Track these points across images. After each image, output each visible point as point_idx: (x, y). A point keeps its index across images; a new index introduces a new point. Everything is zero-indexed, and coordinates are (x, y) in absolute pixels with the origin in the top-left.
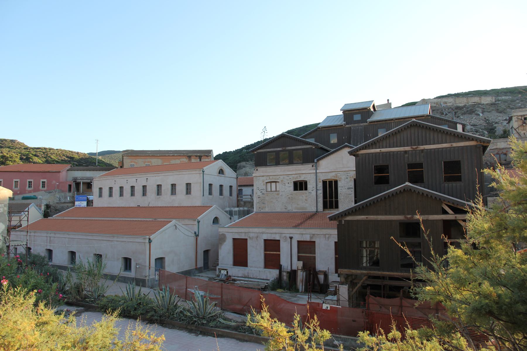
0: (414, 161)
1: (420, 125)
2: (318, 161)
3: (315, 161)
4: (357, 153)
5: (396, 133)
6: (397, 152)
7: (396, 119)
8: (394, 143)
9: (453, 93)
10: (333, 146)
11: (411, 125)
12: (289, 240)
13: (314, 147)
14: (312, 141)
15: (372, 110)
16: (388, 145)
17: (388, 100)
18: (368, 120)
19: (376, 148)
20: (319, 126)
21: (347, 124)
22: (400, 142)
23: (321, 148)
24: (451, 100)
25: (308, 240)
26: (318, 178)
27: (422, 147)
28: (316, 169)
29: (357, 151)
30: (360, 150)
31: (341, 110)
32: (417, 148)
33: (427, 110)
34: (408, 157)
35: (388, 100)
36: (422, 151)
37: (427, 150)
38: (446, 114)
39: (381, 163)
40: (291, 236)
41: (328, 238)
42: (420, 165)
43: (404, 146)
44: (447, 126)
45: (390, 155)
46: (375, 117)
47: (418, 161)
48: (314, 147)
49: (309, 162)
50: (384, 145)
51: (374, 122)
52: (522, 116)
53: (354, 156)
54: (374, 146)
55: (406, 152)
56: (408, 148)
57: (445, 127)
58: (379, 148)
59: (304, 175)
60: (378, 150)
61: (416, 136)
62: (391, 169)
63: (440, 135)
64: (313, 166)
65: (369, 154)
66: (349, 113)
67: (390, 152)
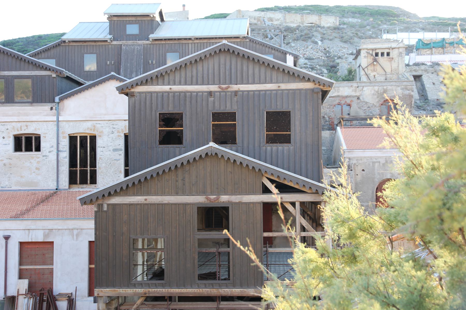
2: (61, 99)
3: (57, 99)
4: (132, 90)
5: (196, 60)
6: (180, 92)
7: (197, 39)
8: (192, 77)
9: (283, 6)
10: (89, 75)
11: (220, 50)
12: (4, 241)
13: (54, 75)
14: (51, 63)
16: (183, 80)
17: (184, 6)
18: (152, 36)
19: (163, 84)
21: (115, 39)
22: (203, 77)
23: (68, 78)
24: (278, 16)
25: (40, 239)
26: (61, 131)
27: (235, 87)
28: (58, 115)
30: (137, 85)
31: (105, 14)
32: (229, 87)
35: (184, 6)
36: (236, 93)
37: (243, 91)
38: (272, 38)
39: (170, 109)
40: (7, 233)
41: (77, 235)
42: (232, 116)
43: (208, 84)
45: (185, 96)
48: (54, 75)
49: (45, 102)
51: (161, 40)
52: (373, 50)
53: (127, 95)
54: (160, 81)
55: (210, 93)
56: (214, 88)
58: (169, 84)
59: (34, 125)
60: (166, 88)
61: (228, 67)
62: (186, 121)
64: (52, 109)
65: (151, 93)
67: (185, 92)
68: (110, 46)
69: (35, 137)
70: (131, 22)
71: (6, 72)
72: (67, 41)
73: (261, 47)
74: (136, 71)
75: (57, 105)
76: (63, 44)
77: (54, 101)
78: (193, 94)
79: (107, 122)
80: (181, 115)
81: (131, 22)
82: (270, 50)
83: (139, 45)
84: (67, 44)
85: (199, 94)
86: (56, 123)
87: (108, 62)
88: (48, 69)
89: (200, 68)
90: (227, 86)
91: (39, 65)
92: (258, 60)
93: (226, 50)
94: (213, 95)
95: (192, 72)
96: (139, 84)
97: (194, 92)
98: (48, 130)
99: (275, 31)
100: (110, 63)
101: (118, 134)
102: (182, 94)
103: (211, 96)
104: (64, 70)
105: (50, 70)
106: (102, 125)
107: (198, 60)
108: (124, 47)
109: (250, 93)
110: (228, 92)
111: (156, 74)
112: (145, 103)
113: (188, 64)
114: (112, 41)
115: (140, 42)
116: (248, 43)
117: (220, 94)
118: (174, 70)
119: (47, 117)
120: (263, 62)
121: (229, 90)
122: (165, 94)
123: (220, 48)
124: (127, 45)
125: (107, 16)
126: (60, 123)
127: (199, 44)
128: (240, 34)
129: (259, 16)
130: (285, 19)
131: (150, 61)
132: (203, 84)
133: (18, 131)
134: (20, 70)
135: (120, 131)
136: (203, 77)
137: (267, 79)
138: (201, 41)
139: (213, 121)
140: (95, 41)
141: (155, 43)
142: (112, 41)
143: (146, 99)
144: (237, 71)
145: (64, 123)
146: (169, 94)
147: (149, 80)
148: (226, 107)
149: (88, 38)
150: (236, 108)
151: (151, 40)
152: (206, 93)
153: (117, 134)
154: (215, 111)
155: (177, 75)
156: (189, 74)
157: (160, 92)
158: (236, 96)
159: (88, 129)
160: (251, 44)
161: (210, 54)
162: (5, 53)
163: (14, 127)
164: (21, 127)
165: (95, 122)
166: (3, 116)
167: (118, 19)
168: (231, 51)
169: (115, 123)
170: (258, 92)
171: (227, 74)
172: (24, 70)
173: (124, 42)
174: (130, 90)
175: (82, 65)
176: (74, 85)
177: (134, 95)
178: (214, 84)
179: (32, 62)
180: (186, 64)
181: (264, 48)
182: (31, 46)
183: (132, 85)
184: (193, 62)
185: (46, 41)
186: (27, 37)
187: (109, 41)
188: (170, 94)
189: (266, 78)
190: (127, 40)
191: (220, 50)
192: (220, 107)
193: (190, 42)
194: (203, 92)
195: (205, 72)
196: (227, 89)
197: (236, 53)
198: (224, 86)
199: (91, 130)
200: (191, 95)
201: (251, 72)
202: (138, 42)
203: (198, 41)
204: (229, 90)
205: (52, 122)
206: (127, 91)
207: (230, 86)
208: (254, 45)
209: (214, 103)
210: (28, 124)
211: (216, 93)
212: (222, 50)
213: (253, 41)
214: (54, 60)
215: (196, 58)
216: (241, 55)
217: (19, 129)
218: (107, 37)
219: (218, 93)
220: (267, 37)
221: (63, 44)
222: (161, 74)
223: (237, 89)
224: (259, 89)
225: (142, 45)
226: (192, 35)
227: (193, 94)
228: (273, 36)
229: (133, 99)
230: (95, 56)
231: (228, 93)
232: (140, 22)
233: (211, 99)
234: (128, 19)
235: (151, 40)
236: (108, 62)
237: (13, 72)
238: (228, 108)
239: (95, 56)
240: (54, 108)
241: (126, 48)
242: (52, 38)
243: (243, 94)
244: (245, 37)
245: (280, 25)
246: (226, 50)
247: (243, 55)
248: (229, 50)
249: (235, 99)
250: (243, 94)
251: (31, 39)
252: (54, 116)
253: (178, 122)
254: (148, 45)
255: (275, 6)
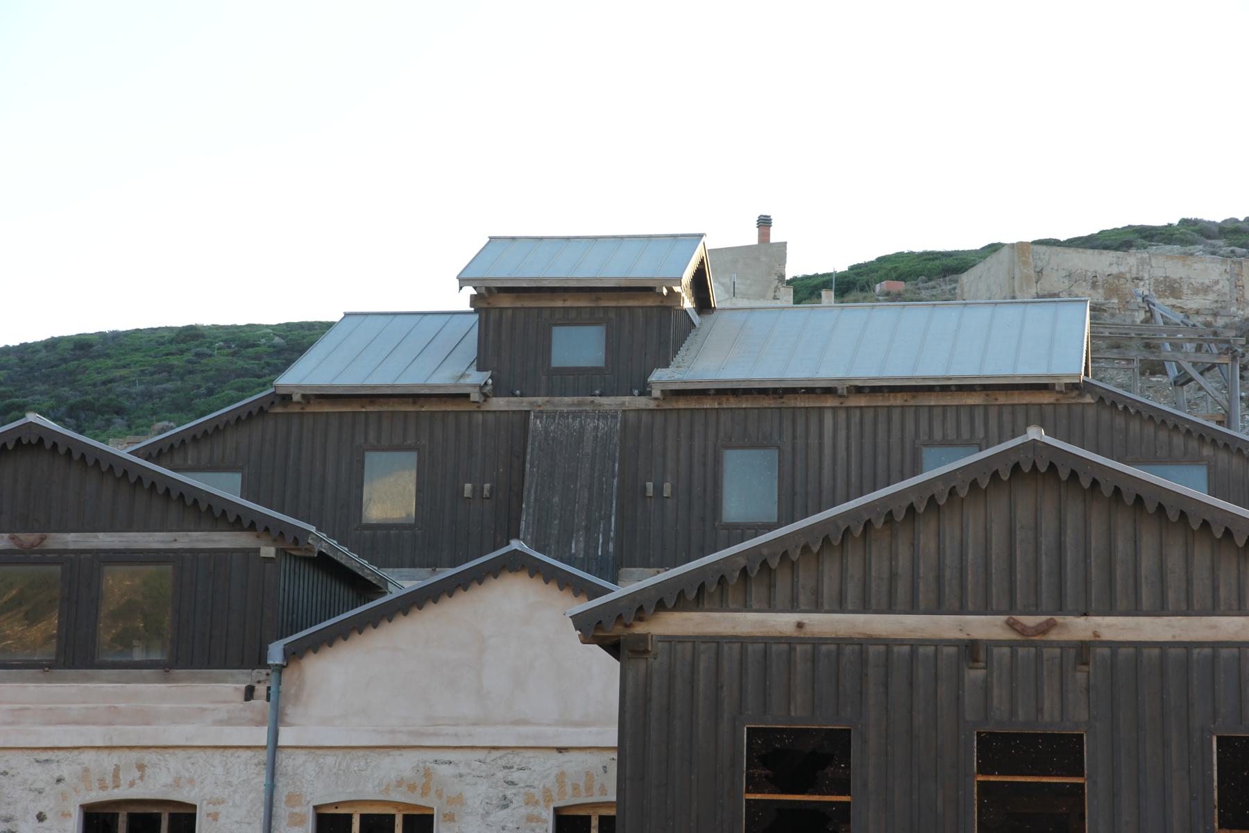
0: (1022, 720)
1: (1074, 475)
2: (294, 654)
3: (275, 652)
4: (640, 629)
5: (911, 509)
6: (840, 642)
7: (859, 390)
8: (893, 576)
9: (1219, 218)
10: (392, 544)
11: (1016, 468)
13: (268, 551)
14: (225, 487)
15: (688, 304)
16: (853, 592)
17: (764, 223)
18: (659, 376)
19: (771, 607)
20: (303, 375)
21: (500, 388)
22: (939, 579)
23: (325, 564)
24: (1205, 270)
26: (283, 789)
27: (1079, 627)
28: (276, 722)
29: (640, 614)
30: (661, 606)
31: (463, 281)
32: (1050, 625)
33: (1054, 344)
34: (987, 688)
35: (764, 223)
36: (1083, 650)
37: (1114, 645)
38: (1183, 380)
39: (797, 712)
42: (1064, 751)
43: (962, 610)
44: (1199, 473)
45: (862, 659)
46: (708, 361)
47: (1051, 717)
48: (268, 551)
49: (225, 665)
50: (829, 587)
51: (702, 393)
53: (614, 648)
54: (757, 591)
55: (971, 650)
56: (986, 627)
57: (1187, 484)
58: (793, 607)
59: (174, 762)
60: (782, 622)
61: (1047, 541)
62: (865, 762)
63: (1202, 555)
64: (249, 693)
65: (717, 642)
66: (516, 311)
67: (863, 643)
68: (480, 416)
69: (173, 817)
70: (573, 314)
71: (71, 537)
72: (296, 398)
73: (1150, 429)
74: (587, 529)
75: (273, 677)
76: (278, 410)
77: (260, 661)
78: (896, 649)
79: (481, 755)
80: (843, 738)
81: (573, 314)
82: (1193, 444)
83: (604, 415)
84: (297, 409)
85: (921, 650)
86: (263, 756)
87: (468, 486)
88: (246, 524)
89: (927, 541)
90: (1043, 618)
91: (210, 507)
92: (1182, 513)
93: (1043, 469)
94: (982, 655)
95: (893, 557)
96: (670, 606)
97: (901, 642)
98: (230, 784)
99: (1199, 348)
100: (474, 489)
101: (530, 810)
102: (848, 649)
103: (976, 660)
104: (313, 529)
105: (252, 527)
106: (463, 770)
107: (921, 509)
108: (536, 424)
109: (1146, 652)
110: (1051, 644)
111: (742, 562)
112: (692, 682)
113: (879, 525)
114: (486, 396)
115: (608, 402)
116: (1091, 412)
117: (1013, 655)
118: (815, 549)
119: (227, 730)
120: (1205, 524)
121: (1053, 636)
122: (774, 648)
123: (1014, 459)
124: (552, 415)
125: (470, 291)
126: (282, 756)
127: (869, 416)
128: (1056, 371)
129: (1114, 270)
130: (1238, 286)
131: (650, 485)
132: (938, 608)
133: (103, 787)
134: (129, 529)
135: (538, 795)
136: (939, 579)
137: (1223, 593)
138: (879, 401)
139: (982, 770)
140: (415, 398)
141: (675, 406)
142: (486, 396)
143: (693, 665)
144: (1087, 555)
145: (301, 757)
146: (791, 650)
147: (712, 588)
148: (1039, 710)
149: (388, 381)
150: (1083, 715)
151: (656, 393)
152: (953, 650)
153: (524, 811)
154: (988, 729)
155: (830, 570)
156: (879, 567)
157: (754, 639)
158: (1086, 663)
159: (400, 783)
160: (1106, 415)
161: (974, 485)
162: (76, 456)
163: (86, 770)
164: (117, 769)
165: (430, 756)
166: (49, 723)
167: (518, 304)
168: (1064, 474)
169: (516, 759)
170: (1181, 651)
171: (1044, 568)
172: (146, 528)
173: (540, 400)
174: (627, 626)
175: (355, 502)
176: (341, 592)
177: (646, 651)
178: (986, 609)
179: (181, 496)
180: (868, 524)
181: (1163, 435)
182: (42, 388)
183: (641, 609)
184: (900, 516)
185: (110, 362)
186: (24, 347)
187: (475, 396)
188: (799, 648)
189: (1215, 590)
190: (550, 393)
191: (1016, 468)
192: (1013, 712)
193: (830, 402)
194: (938, 643)
195: (951, 559)
196: (1044, 632)
197: (1086, 483)
198: (1030, 621)
199: (412, 788)
200: (888, 653)
201: (1147, 563)
202: (598, 400)
203: (862, 401)
204: (1053, 636)
205: (249, 753)
206: (618, 630)
207: (1059, 619)
208: (1120, 421)
209: (987, 688)
210: (148, 757)
211: (996, 651)
212: (1026, 468)
213: (1114, 404)
214: (237, 477)
215: (913, 499)
216: (1107, 491)
217: (109, 781)
218: (468, 381)
219: (1006, 650)
220: (1156, 368)
221: (278, 410)
222: (764, 564)
223: (1087, 636)
224: (1185, 637)
225: (615, 417)
226: (840, 374)
227: (896, 649)
228: (1194, 373)
229: (642, 665)
230: (412, 457)
231: (1047, 652)
232: (612, 315)
233: (975, 675)
234: (559, 304)
235: (656, 393)
236: (468, 486)
237: (101, 535)
238: (1047, 717)
239: (412, 457)
240: (261, 690)
241: (546, 428)
242: (137, 350)
243: (1114, 655)
244: (1074, 387)
245: (1215, 315)
246: (1043, 469)
247: (1117, 491)
248: (1052, 467)
249: (1081, 676)
250: (1114, 655)
251: (44, 353)
252: (259, 724)
253: (829, 770)
254: (644, 417)
255: (1184, 222)
